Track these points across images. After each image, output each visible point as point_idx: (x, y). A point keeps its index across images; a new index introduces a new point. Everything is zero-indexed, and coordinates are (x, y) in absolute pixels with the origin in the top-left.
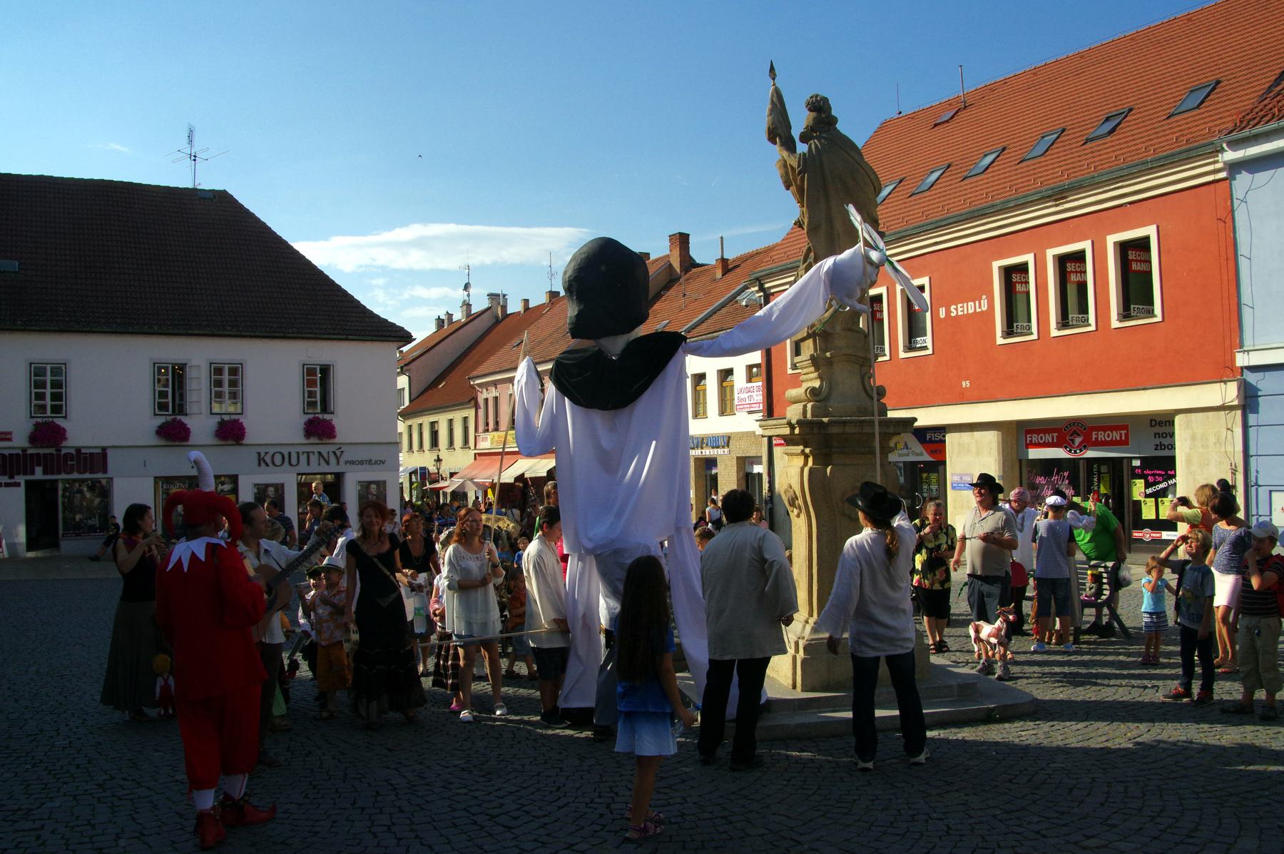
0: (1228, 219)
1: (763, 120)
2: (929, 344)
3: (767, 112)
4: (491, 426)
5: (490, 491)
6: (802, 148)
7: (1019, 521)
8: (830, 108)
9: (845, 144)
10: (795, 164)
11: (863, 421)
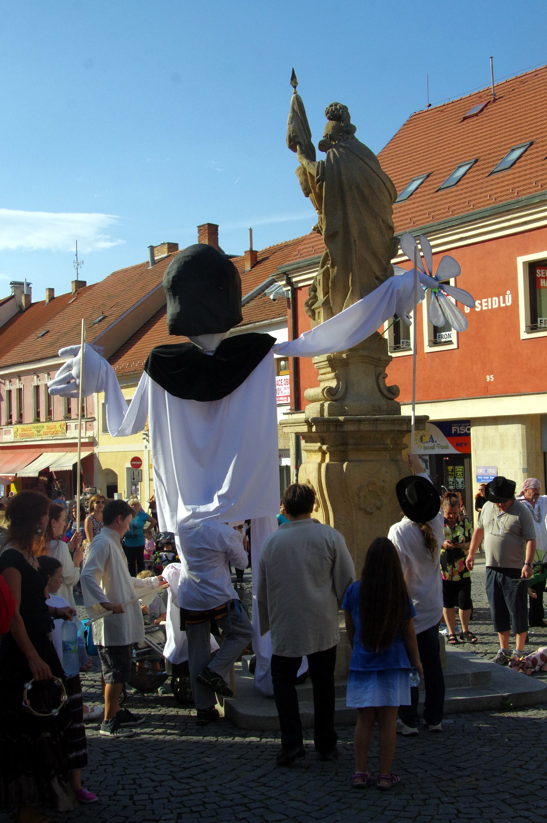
1: (283, 128)
2: (454, 338)
3: (288, 120)
4: (15, 418)
5: (13, 486)
6: (321, 156)
7: (536, 512)
8: (348, 117)
9: (362, 153)
10: (314, 173)
11: (377, 420)
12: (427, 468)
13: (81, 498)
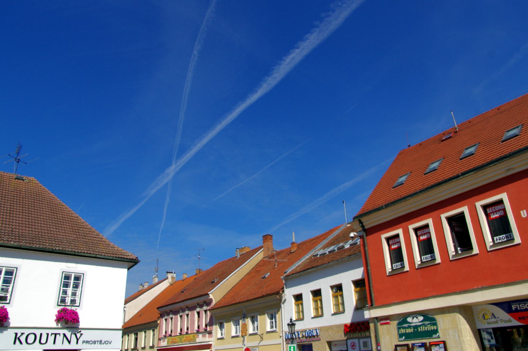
0: (368, 229)
12: (492, 338)
13: (73, 212)
